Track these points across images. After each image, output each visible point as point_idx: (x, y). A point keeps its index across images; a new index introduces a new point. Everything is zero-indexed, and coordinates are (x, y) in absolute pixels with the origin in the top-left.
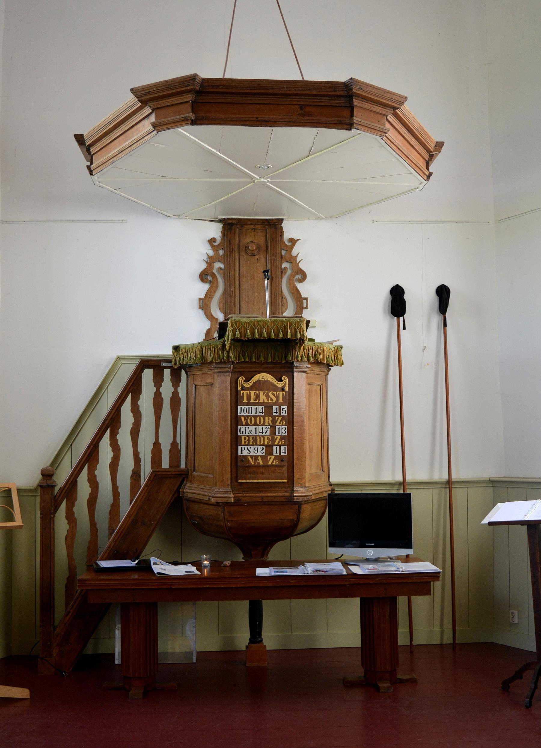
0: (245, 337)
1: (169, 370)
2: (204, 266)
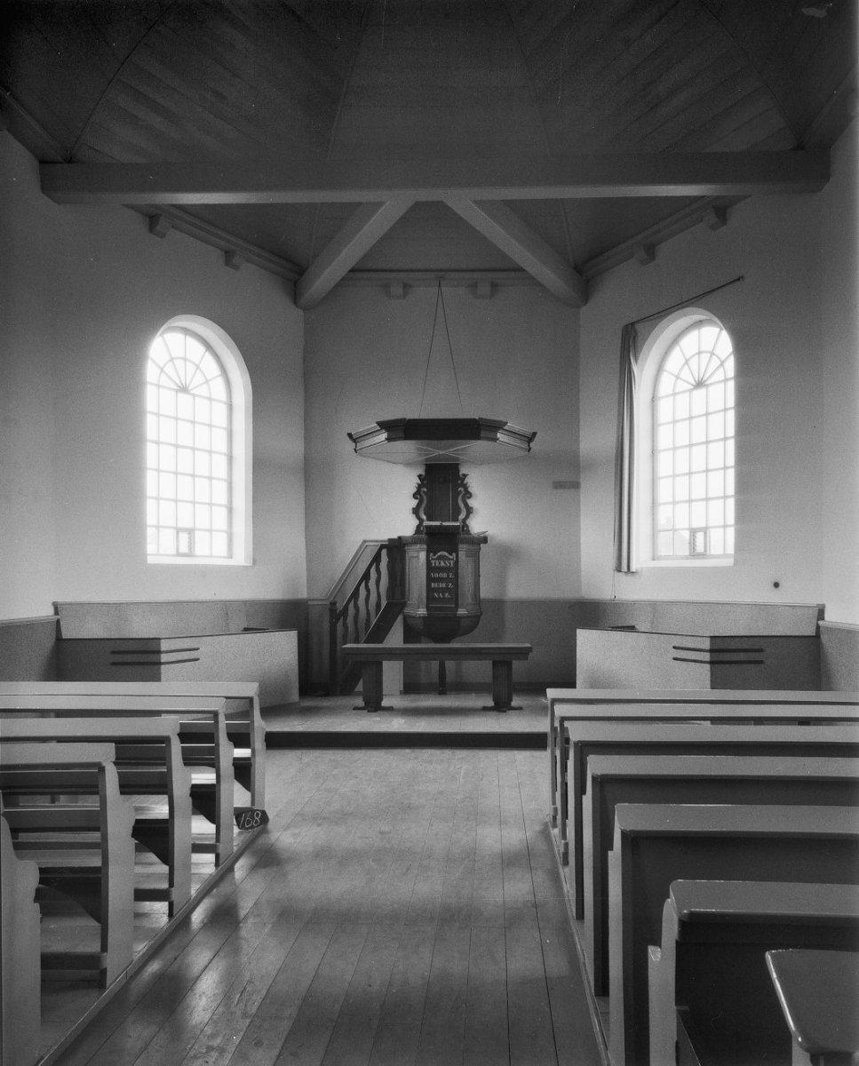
0: (190, 555)
1: (214, 782)
2: (415, 490)
